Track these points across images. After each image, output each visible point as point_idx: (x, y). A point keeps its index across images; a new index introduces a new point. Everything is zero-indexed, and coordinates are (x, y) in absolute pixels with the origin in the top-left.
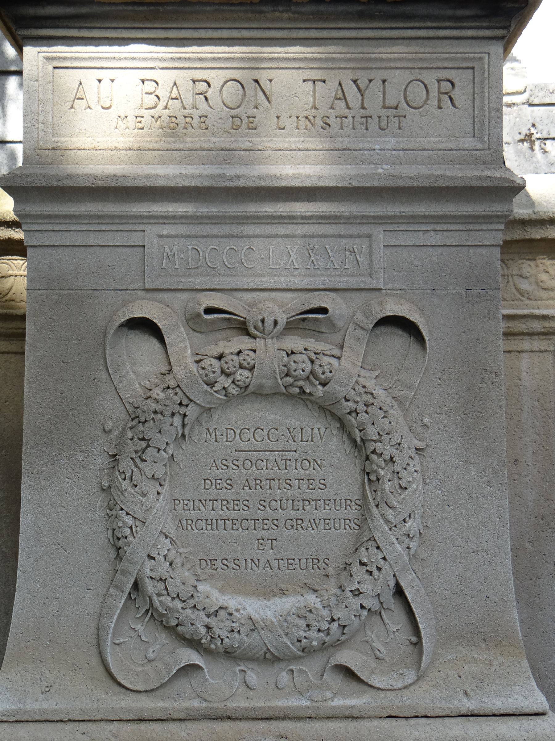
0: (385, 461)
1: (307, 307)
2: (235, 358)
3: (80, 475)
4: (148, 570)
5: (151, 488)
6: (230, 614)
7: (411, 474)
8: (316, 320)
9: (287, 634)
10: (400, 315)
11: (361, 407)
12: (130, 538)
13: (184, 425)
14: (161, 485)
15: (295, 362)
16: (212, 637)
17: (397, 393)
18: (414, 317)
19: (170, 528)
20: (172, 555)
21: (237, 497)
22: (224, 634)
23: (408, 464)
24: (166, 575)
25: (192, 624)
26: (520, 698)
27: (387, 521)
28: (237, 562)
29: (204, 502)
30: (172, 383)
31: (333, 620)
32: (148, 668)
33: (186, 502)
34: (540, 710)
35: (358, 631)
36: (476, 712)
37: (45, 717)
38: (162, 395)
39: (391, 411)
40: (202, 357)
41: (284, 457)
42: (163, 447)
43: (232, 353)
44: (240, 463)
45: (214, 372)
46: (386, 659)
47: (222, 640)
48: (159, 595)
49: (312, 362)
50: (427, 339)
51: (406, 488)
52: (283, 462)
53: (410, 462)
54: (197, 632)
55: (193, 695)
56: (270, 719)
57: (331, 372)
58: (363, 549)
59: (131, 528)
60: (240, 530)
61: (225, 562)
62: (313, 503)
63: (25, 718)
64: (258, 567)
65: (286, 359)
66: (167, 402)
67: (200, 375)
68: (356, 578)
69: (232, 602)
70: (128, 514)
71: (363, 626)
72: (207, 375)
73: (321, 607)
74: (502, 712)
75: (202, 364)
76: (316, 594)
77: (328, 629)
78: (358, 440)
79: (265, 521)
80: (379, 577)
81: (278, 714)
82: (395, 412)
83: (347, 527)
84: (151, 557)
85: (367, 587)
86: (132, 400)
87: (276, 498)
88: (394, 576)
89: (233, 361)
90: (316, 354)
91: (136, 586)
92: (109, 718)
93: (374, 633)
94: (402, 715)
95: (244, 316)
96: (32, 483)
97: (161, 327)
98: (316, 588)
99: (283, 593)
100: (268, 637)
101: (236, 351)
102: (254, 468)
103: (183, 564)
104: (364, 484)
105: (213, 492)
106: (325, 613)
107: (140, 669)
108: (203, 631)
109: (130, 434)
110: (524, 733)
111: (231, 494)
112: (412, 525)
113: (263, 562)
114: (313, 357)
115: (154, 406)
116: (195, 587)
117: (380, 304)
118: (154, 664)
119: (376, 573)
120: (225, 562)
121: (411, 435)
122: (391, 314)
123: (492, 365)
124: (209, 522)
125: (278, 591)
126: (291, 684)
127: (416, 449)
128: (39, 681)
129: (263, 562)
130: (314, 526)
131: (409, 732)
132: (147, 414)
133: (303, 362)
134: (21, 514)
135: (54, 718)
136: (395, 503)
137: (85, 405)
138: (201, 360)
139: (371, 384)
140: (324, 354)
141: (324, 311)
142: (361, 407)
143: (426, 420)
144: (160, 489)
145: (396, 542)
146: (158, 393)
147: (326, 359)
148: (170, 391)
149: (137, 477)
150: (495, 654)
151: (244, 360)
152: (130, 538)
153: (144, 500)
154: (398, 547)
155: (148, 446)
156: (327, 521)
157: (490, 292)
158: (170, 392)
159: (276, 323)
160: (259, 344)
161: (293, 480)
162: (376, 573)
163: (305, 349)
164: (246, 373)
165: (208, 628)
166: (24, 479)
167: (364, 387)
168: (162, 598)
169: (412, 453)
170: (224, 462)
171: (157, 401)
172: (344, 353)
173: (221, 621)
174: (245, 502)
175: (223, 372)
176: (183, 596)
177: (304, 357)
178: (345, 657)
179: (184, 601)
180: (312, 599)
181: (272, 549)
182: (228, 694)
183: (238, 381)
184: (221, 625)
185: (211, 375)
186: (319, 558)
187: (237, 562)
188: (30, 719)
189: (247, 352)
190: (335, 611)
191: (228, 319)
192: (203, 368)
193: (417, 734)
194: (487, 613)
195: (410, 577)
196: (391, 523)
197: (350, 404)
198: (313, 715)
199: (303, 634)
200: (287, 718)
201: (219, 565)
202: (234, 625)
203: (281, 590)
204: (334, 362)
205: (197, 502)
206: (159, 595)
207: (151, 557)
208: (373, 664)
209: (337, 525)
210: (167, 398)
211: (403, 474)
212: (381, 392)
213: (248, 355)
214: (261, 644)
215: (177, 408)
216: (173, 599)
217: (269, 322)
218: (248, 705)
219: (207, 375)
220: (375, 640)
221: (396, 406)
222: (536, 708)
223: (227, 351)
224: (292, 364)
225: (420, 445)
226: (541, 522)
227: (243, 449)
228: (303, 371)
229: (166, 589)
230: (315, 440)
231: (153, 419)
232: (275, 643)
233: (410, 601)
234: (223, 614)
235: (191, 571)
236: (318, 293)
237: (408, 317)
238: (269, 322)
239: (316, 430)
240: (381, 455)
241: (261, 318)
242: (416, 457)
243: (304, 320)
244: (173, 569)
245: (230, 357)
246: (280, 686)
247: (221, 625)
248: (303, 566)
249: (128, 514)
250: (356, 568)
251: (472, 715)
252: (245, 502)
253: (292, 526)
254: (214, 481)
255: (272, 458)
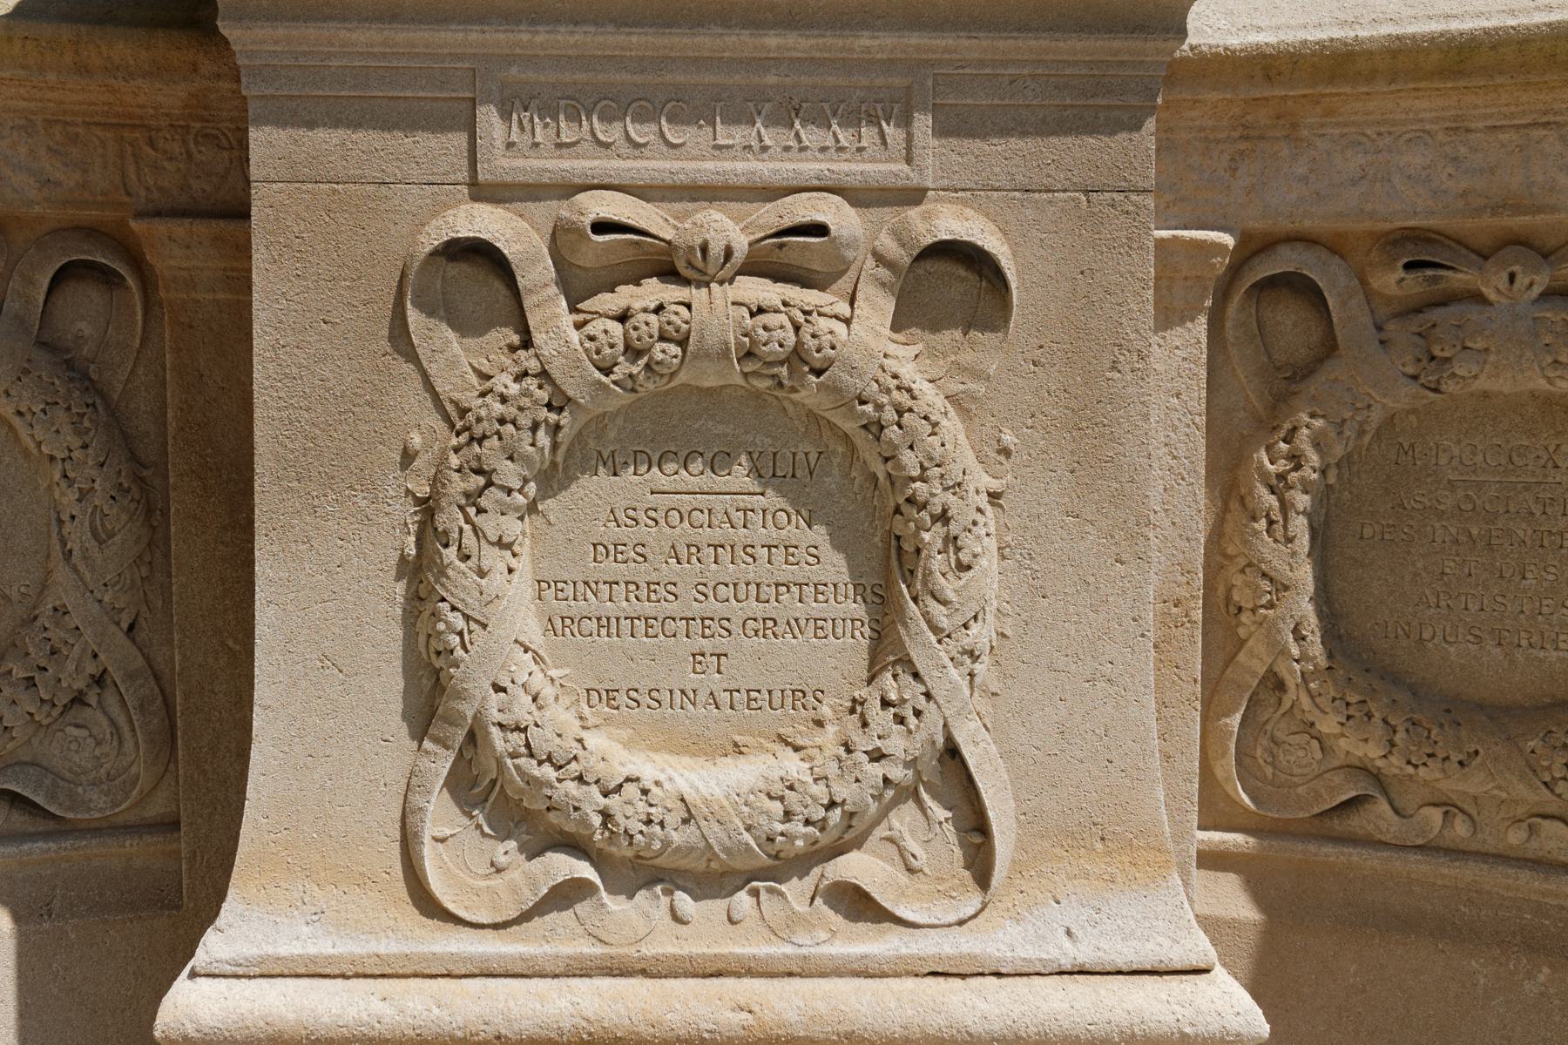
0: (932, 516)
1: (787, 222)
2: (653, 318)
3: (363, 534)
4: (495, 711)
5: (493, 558)
6: (645, 792)
7: (978, 538)
8: (806, 246)
9: (748, 829)
10: (965, 238)
11: (889, 415)
12: (459, 652)
13: (555, 446)
14: (514, 555)
15: (765, 328)
16: (612, 832)
17: (955, 387)
18: (993, 243)
19: (533, 632)
20: (538, 681)
21: (654, 577)
22: (635, 826)
23: (975, 523)
24: (526, 720)
25: (576, 809)
26: (1167, 943)
27: (935, 629)
28: (654, 694)
29: (593, 586)
30: (533, 365)
31: (832, 804)
32: (497, 882)
33: (560, 585)
34: (1203, 966)
35: (877, 822)
36: (1087, 967)
37: (313, 969)
38: (514, 389)
39: (944, 422)
40: (589, 317)
41: (742, 505)
42: (517, 484)
43: (645, 310)
44: (660, 516)
45: (612, 346)
46: (926, 870)
47: (632, 837)
48: (514, 756)
49: (797, 328)
50: (1013, 286)
51: (969, 568)
52: (741, 514)
53: (979, 517)
54: (585, 822)
55: (580, 930)
56: (719, 974)
57: (833, 348)
58: (889, 675)
59: (461, 634)
60: (662, 637)
61: (633, 694)
62: (795, 589)
63: (278, 971)
64: (694, 704)
65: (748, 322)
66: (525, 402)
67: (586, 351)
68: (875, 729)
69: (648, 767)
70: (454, 609)
71: (884, 814)
72: (598, 352)
73: (810, 780)
74: (1135, 967)
75: (589, 329)
76: (802, 754)
77: (824, 819)
78: (881, 476)
79: (707, 622)
80: (918, 727)
81: (733, 967)
82: (952, 425)
83: (857, 633)
84: (499, 689)
85: (896, 744)
86: (456, 395)
87: (727, 580)
88: (945, 725)
89: (647, 324)
90: (805, 313)
91: (471, 737)
92: (428, 971)
93: (903, 820)
94: (955, 971)
95: (668, 237)
96: (275, 548)
97: (510, 257)
98: (800, 742)
99: (738, 749)
100: (715, 834)
101: (652, 306)
102: (686, 524)
103: (557, 698)
104: (888, 558)
105: (610, 568)
106: (819, 790)
107: (483, 883)
108: (597, 820)
109: (455, 461)
110: (1177, 1008)
111: (643, 573)
112: (981, 635)
113: (702, 696)
114: (801, 318)
115: (498, 408)
116: (580, 741)
117: (927, 217)
118: (507, 876)
119: (912, 721)
120: (633, 694)
121: (979, 467)
122: (948, 237)
123: (1133, 336)
124: (603, 622)
125: (730, 748)
126: (755, 913)
127: (989, 494)
128: (299, 904)
129: (702, 696)
130: (797, 631)
131: (969, 1003)
132: (485, 424)
133: (782, 327)
134: (257, 603)
135: (327, 971)
136: (951, 596)
137: (368, 403)
138: (585, 323)
139: (908, 372)
140: (820, 314)
141: (820, 230)
142: (889, 415)
143: (1008, 438)
144: (513, 563)
145: (950, 664)
146: (505, 382)
147: (823, 324)
148: (529, 380)
149: (469, 539)
150: (1121, 862)
151: (669, 323)
152: (459, 652)
153: (483, 582)
154: (954, 673)
155: (489, 484)
156: (820, 623)
157: (1134, 197)
158: (531, 383)
159: (729, 253)
160: (697, 295)
161: (758, 548)
162: (912, 721)
163: (785, 304)
164: (674, 349)
165: (606, 816)
166: (260, 541)
167: (895, 376)
168: (522, 761)
169: (983, 501)
170: (631, 512)
171: (504, 399)
172: (857, 312)
173: (629, 803)
174: (670, 587)
175: (628, 348)
176: (559, 758)
177: (783, 318)
178: (855, 867)
179: (561, 767)
180: (793, 766)
181: (719, 672)
182: (642, 932)
183: (657, 363)
184: (630, 811)
185: (608, 351)
186: (805, 688)
187: (654, 694)
188: (286, 972)
189: (674, 308)
190: (835, 787)
191: (637, 243)
192: (592, 339)
193: (983, 1006)
194: (1107, 790)
195: (972, 725)
196: (943, 630)
197: (869, 408)
198: (795, 969)
199: (780, 827)
200: (750, 973)
201: (622, 699)
202: (653, 810)
203: (736, 745)
204: (840, 328)
205: (581, 587)
206: (514, 756)
207: (499, 689)
208: (903, 878)
209: (839, 631)
210: (526, 393)
211: (966, 540)
212: (926, 386)
213: (677, 313)
214: (702, 845)
215: (544, 413)
216: (540, 763)
217: (716, 249)
218: (679, 951)
219: (598, 352)
220: (907, 835)
221: (952, 412)
222: (1195, 961)
223: (637, 305)
224: (761, 331)
225: (995, 485)
226: (1174, 610)
227: (666, 488)
228: (781, 345)
229: (528, 745)
230: (799, 473)
231: (498, 433)
232: (728, 843)
233: (972, 769)
234: (631, 790)
235: (573, 710)
236: (805, 195)
237: (980, 243)
238: (716, 249)
239: (801, 456)
240: (924, 506)
241: (699, 241)
242: (988, 509)
243: (781, 246)
244: (540, 708)
245: (642, 317)
246: (736, 917)
247: (630, 811)
248: (777, 702)
249: (454, 609)
250: (874, 710)
251: (1081, 973)
252: (670, 587)
253: (756, 632)
254: (611, 548)
255: (719, 508)
